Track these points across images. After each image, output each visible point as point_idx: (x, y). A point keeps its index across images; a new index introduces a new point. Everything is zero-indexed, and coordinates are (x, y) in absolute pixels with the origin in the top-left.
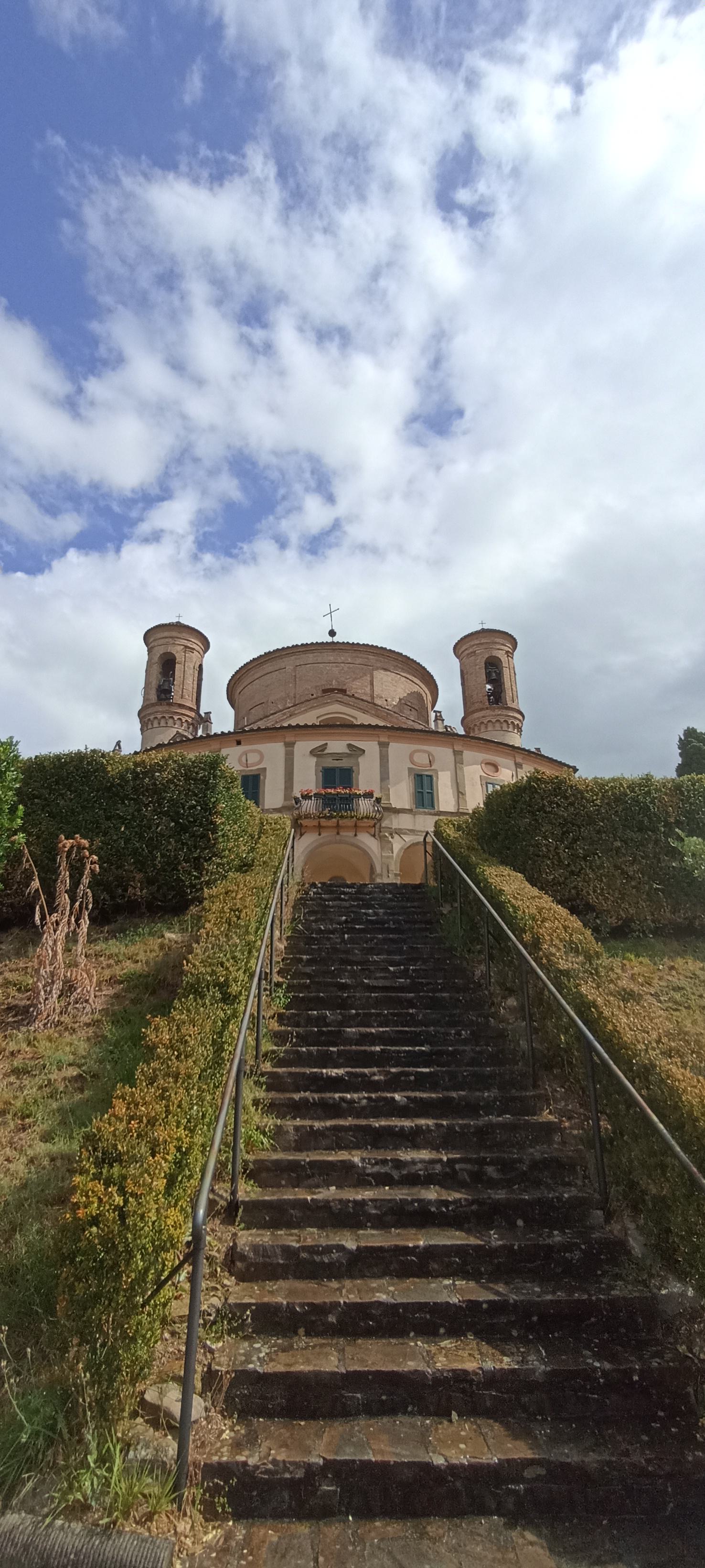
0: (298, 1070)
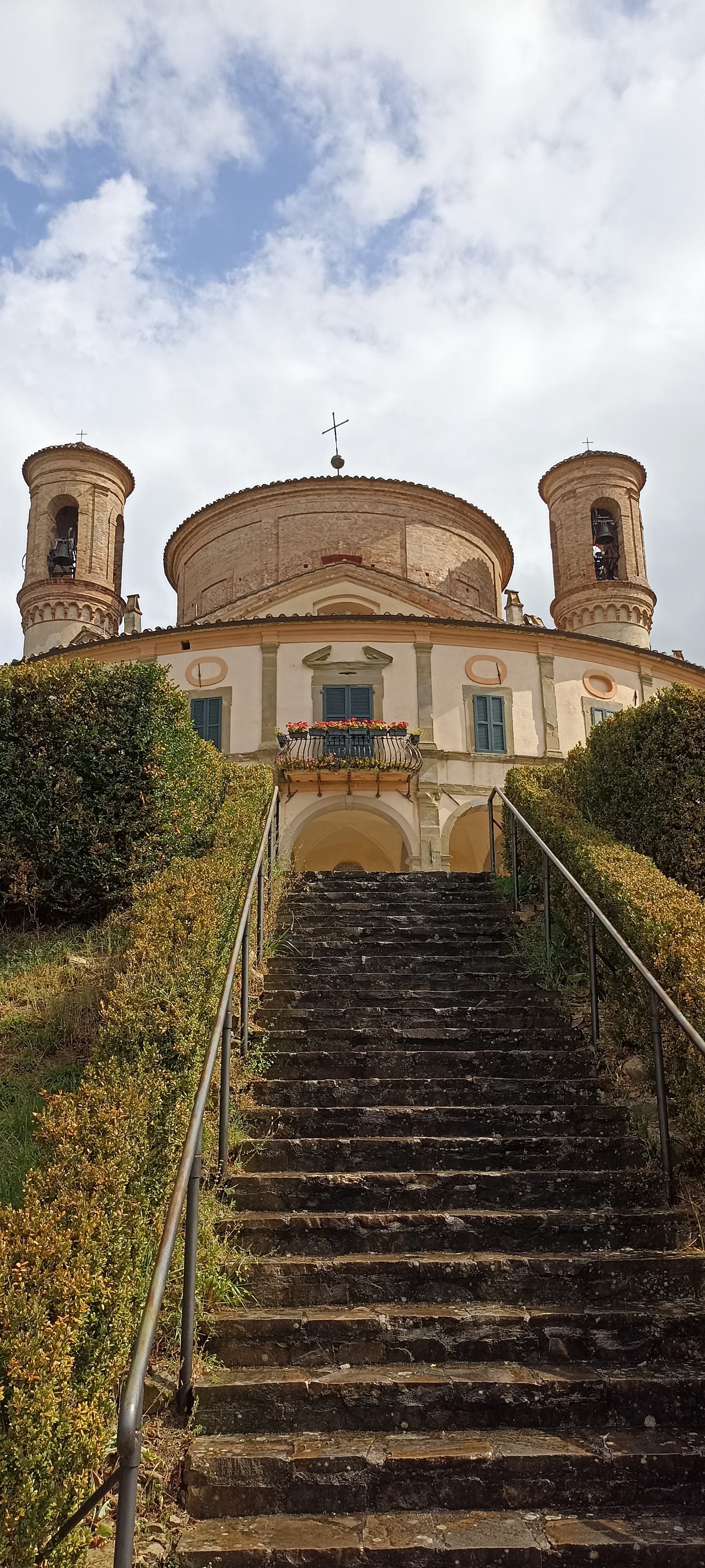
0: (287, 1175)
